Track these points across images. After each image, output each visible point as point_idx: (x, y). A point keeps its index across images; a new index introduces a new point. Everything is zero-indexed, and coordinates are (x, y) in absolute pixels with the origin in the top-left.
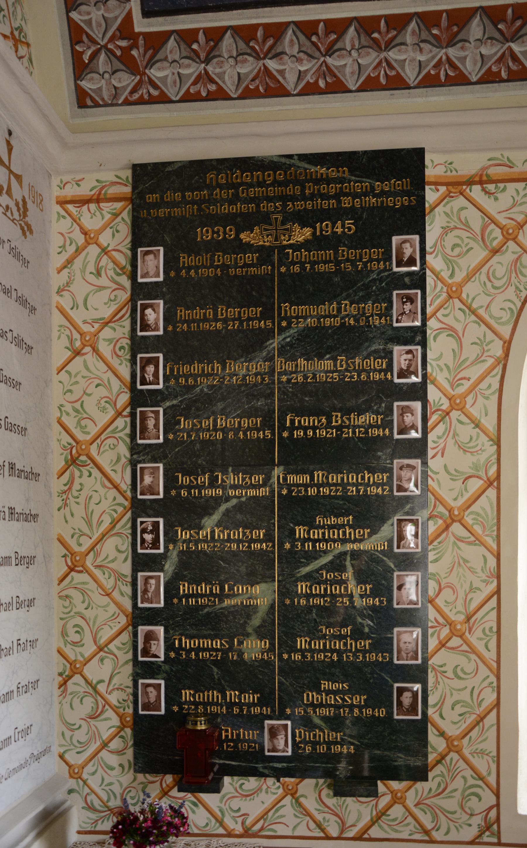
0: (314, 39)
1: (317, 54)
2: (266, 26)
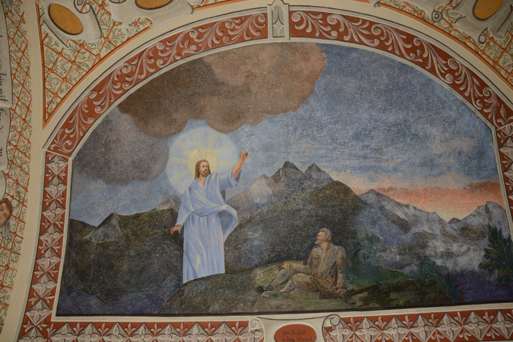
0: (74, 329)
1: (126, 336)
2: (107, 323)
